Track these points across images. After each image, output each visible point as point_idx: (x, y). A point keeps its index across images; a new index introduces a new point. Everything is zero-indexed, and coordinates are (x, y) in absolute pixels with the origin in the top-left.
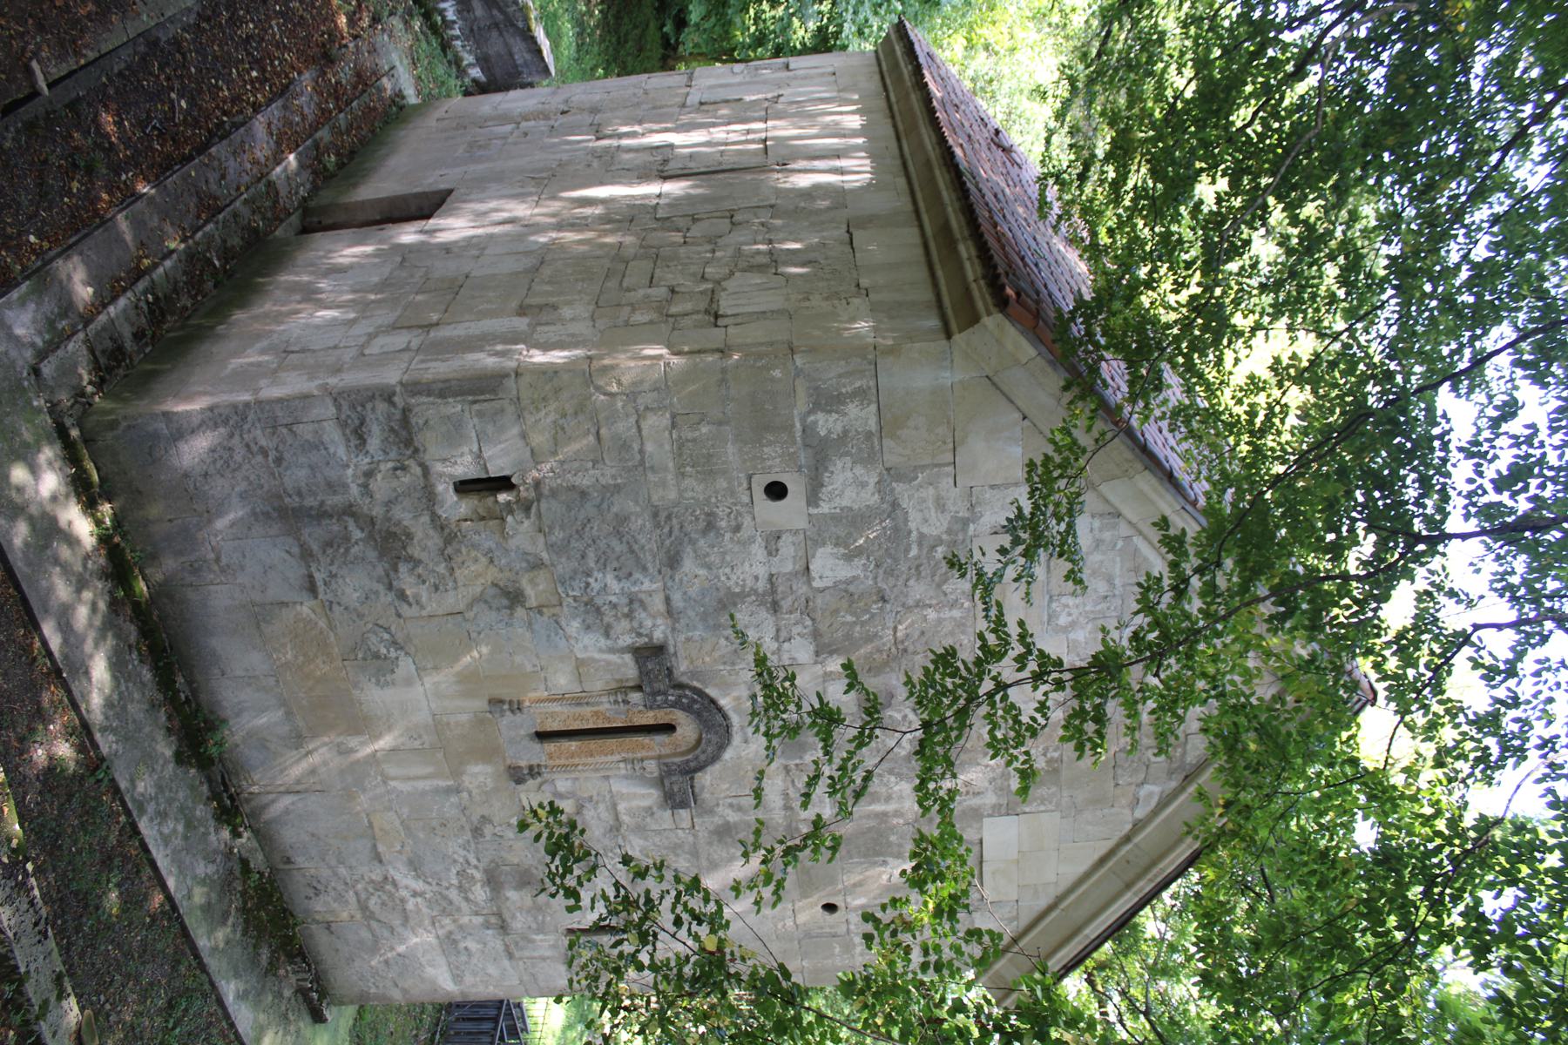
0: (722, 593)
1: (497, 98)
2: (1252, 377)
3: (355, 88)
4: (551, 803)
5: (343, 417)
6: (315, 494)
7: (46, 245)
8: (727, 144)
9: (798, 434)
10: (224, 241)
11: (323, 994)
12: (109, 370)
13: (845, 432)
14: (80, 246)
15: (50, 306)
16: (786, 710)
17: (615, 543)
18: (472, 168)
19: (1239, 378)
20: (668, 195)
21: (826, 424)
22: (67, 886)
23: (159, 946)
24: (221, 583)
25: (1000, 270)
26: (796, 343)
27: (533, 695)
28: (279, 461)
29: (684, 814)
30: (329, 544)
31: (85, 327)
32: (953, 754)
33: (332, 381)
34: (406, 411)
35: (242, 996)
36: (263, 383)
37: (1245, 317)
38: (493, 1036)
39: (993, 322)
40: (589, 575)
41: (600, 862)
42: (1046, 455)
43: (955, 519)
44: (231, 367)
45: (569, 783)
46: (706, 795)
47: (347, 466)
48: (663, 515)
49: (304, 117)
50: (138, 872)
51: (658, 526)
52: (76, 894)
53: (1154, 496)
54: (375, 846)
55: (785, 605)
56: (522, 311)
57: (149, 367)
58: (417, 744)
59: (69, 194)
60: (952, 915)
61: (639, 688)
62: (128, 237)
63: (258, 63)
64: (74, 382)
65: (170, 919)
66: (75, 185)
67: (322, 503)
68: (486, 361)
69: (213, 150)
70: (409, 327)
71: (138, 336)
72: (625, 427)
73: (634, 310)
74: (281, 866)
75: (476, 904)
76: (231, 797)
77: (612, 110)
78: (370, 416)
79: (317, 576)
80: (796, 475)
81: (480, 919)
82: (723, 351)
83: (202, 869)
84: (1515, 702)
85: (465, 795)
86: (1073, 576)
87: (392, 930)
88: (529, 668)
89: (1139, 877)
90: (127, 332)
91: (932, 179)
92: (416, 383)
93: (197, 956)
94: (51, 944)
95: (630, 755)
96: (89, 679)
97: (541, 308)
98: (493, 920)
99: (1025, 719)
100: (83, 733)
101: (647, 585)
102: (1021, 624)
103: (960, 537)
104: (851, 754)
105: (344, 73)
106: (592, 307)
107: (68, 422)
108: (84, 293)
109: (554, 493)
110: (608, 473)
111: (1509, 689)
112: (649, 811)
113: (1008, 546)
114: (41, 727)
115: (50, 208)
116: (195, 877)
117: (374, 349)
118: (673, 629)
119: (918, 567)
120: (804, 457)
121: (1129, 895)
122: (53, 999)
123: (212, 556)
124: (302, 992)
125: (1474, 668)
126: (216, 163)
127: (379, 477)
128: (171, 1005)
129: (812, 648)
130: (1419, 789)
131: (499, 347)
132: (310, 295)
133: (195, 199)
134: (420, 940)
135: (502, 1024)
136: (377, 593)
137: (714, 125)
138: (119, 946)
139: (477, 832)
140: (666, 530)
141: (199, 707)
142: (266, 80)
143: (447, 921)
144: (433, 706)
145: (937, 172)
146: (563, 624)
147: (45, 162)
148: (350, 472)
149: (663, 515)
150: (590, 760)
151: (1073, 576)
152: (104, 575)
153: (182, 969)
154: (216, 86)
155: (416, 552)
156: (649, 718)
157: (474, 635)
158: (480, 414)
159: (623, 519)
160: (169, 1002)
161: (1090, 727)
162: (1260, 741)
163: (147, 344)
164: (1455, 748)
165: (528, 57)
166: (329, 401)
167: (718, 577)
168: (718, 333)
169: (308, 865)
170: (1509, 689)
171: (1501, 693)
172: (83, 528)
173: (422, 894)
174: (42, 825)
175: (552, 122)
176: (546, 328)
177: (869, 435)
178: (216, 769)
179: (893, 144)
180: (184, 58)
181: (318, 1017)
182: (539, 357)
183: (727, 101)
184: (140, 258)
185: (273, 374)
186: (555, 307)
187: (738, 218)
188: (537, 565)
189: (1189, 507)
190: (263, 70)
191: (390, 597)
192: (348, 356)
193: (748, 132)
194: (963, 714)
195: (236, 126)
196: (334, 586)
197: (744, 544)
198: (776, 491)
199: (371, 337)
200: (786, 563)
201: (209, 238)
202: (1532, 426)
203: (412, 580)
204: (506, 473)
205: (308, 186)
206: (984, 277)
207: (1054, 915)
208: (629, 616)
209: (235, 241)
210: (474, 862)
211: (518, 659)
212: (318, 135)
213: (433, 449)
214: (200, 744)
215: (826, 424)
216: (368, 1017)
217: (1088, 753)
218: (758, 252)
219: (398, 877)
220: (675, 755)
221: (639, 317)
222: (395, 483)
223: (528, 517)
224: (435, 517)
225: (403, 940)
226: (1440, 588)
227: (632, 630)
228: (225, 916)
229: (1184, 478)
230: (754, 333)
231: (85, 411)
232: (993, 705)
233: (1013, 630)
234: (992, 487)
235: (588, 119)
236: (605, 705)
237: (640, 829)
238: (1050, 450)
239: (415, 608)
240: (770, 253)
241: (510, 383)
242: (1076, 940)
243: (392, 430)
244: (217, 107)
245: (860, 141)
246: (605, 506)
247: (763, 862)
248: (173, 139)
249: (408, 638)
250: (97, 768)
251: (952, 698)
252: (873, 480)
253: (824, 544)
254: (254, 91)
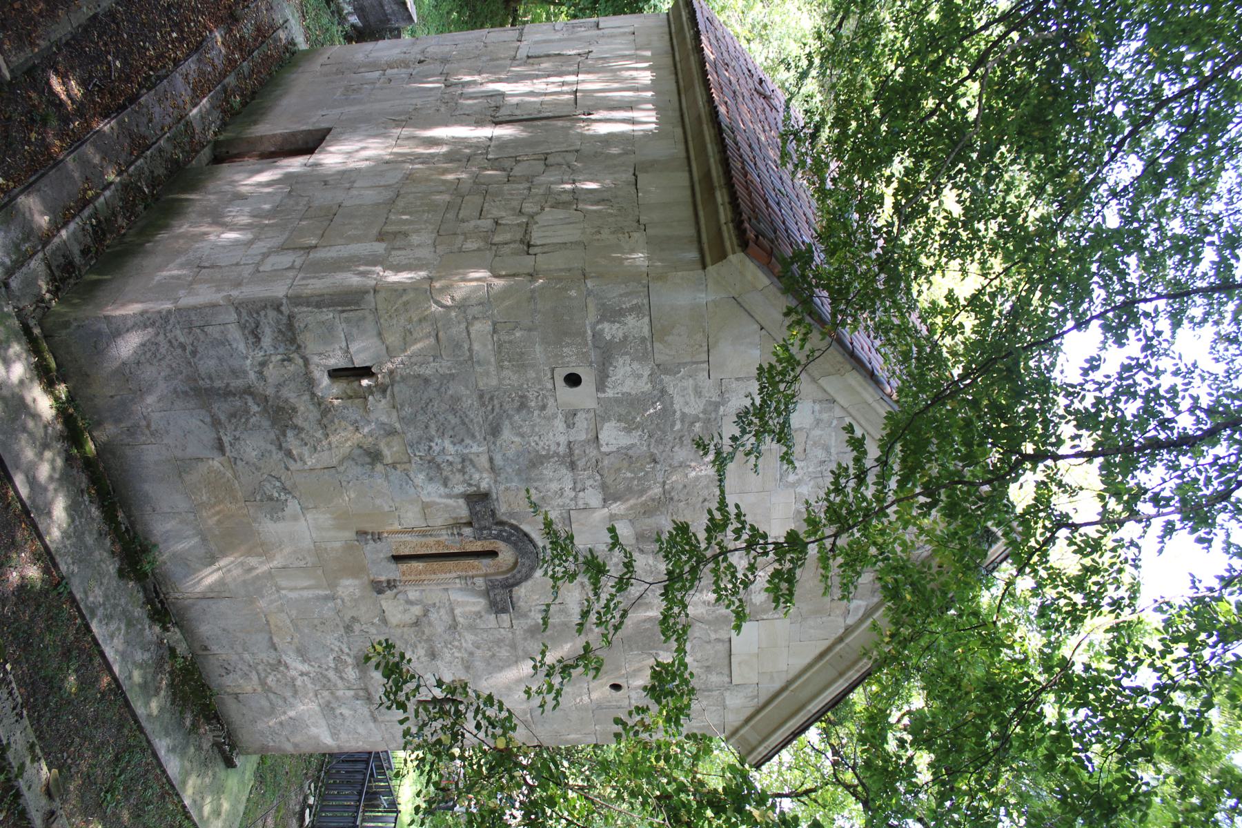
0: (532, 455)
1: (368, 46)
2: (933, 303)
3: (255, 40)
4: (387, 641)
5: (243, 321)
6: (222, 379)
7: (11, 184)
8: (546, 94)
9: (590, 338)
10: (152, 172)
11: (233, 747)
12: (63, 280)
13: (625, 337)
14: (37, 186)
15: (15, 233)
16: (566, 561)
17: (451, 417)
18: (347, 109)
19: (923, 303)
20: (498, 138)
21: (610, 331)
22: (37, 673)
23: (108, 715)
24: (152, 443)
25: (745, 216)
26: (588, 270)
27: (389, 528)
28: (194, 353)
29: (505, 617)
30: (233, 415)
31: (43, 248)
32: (687, 599)
33: (235, 293)
34: (291, 317)
35: (172, 750)
36: (181, 293)
37: (928, 258)
38: (365, 774)
39: (736, 259)
40: (431, 441)
41: (422, 683)
42: (770, 365)
43: (710, 403)
44: (157, 278)
45: (418, 593)
46: (521, 604)
47: (246, 359)
48: (487, 397)
49: (214, 67)
50: (91, 660)
51: (483, 405)
52: (44, 679)
53: (859, 389)
54: (271, 638)
55: (581, 464)
56: (381, 237)
57: (95, 277)
58: (302, 564)
59: (29, 142)
60: (677, 723)
61: (470, 524)
62: (76, 175)
63: (177, 26)
64: (36, 291)
65: (116, 694)
66: (33, 136)
67: (228, 385)
68: (353, 280)
69: (142, 100)
70: (294, 249)
71: (85, 252)
72: (458, 330)
73: (466, 239)
74: (200, 652)
75: (348, 681)
76: (161, 602)
77: (459, 61)
78: (263, 321)
79: (224, 438)
80: (588, 369)
81: (352, 693)
82: (532, 276)
83: (140, 656)
84: (1095, 570)
85: (339, 601)
86: (786, 458)
87: (285, 700)
89: (849, 668)
90: (76, 250)
91: (701, 133)
92: (298, 297)
93: (136, 721)
94: (26, 722)
95: (464, 574)
96: (51, 517)
97: (395, 234)
98: (361, 693)
99: (740, 575)
100: (47, 558)
101: (476, 449)
102: (737, 506)
103: (713, 416)
104: (613, 596)
105: (246, 29)
106: (434, 235)
107: (32, 323)
108: (43, 221)
109: (403, 379)
110: (445, 365)
111: (1093, 560)
112: (479, 615)
113: (738, 434)
114: (15, 556)
115: (14, 155)
116: (134, 663)
117: (266, 267)
118: (496, 481)
119: (681, 438)
120: (593, 355)
121: (841, 681)
122: (28, 762)
123: (143, 423)
124: (217, 745)
125: (1069, 545)
126: (145, 110)
127: (271, 366)
128: (117, 759)
129: (601, 496)
130: (1014, 641)
131: (362, 268)
132: (218, 220)
133: (128, 140)
134: (306, 708)
135: (372, 764)
136: (270, 452)
137: (537, 77)
138: (77, 716)
139: (348, 628)
140: (490, 408)
141: (136, 536)
142: (184, 39)
143: (326, 693)
144: (314, 535)
145: (705, 127)
146: (412, 476)
147: (9, 119)
148: (248, 362)
149: (487, 397)
150: (433, 577)
151: (786, 458)
152: (61, 437)
153: (126, 731)
154: (144, 47)
155: (299, 421)
156: (478, 546)
157: (344, 484)
158: (347, 321)
159: (456, 399)
160: (116, 756)
161: (784, 585)
162: (913, 593)
163: (92, 258)
164: (1052, 604)
165: (395, 7)
166: (232, 309)
167: (528, 443)
168: (529, 260)
169: (221, 651)
170: (1093, 560)
171: (1087, 562)
172: (44, 404)
173: (307, 674)
174: (17, 629)
175: (410, 70)
176: (399, 253)
177: (643, 340)
178: (150, 581)
179: (675, 98)
180: (118, 27)
181: (230, 764)
182: (393, 277)
183: (548, 56)
184: (85, 191)
185: (190, 286)
186: (406, 235)
187: (551, 160)
188: (391, 432)
189: (886, 398)
190: (181, 31)
191: (281, 455)
192: (247, 272)
193: (563, 84)
194: (694, 570)
195: (160, 79)
196: (237, 446)
197: (549, 419)
198: (573, 380)
199: (265, 256)
200: (581, 433)
201: (140, 171)
202: (1108, 377)
203: (298, 442)
204: (368, 364)
205: (218, 123)
206: (732, 221)
207: (785, 694)
208: (463, 471)
209: (161, 171)
210: (346, 650)
211: (378, 502)
212: (227, 80)
213: (311, 346)
214: (137, 563)
215: (610, 331)
216: (269, 762)
217: (782, 605)
218: (565, 191)
219: (289, 661)
220: (497, 574)
221: (471, 245)
222: (283, 371)
223: (385, 397)
224: (313, 395)
225: (292, 706)
226: (1052, 480)
227: (464, 481)
228: (157, 691)
229: (882, 374)
230: (557, 261)
231: (44, 314)
232: (717, 564)
233: (732, 510)
234: (737, 379)
235: (438, 68)
236: (444, 537)
237: (472, 628)
238: (773, 361)
239: (300, 463)
240: (573, 191)
241: (370, 297)
242: (802, 713)
243: (280, 331)
244: (145, 64)
245: (649, 94)
246: (443, 389)
247: (547, 675)
248: (111, 94)
249: (295, 485)
250: (59, 583)
251: (686, 558)
252: (647, 373)
253: (609, 420)
254: (175, 49)
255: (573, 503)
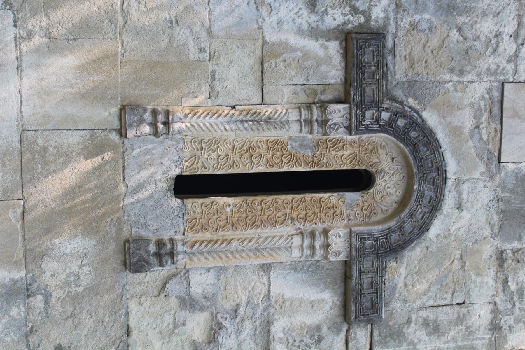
85: (38, 301)
255: (510, 67)
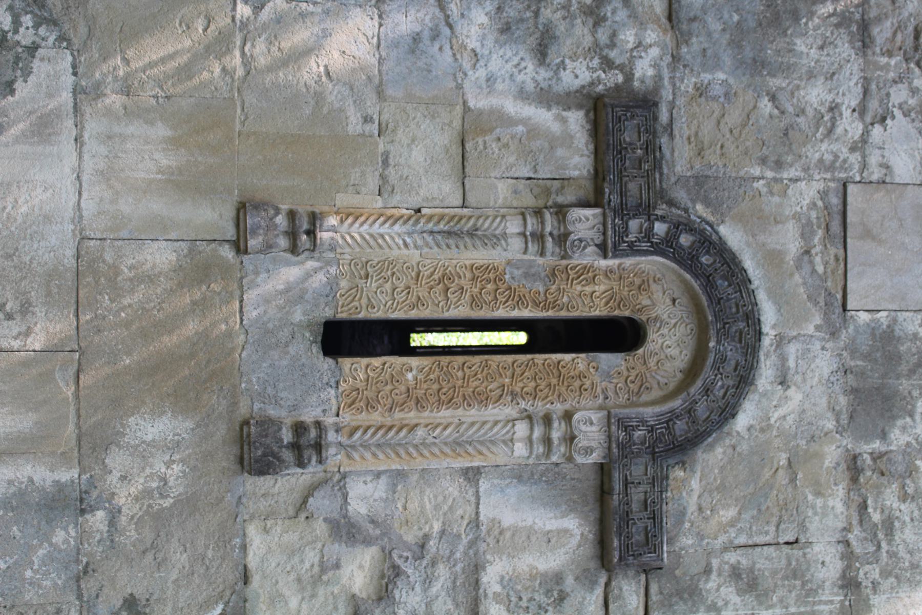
27: (343, 200)
88: (354, 124)
144: (89, 206)
227: (595, 48)
